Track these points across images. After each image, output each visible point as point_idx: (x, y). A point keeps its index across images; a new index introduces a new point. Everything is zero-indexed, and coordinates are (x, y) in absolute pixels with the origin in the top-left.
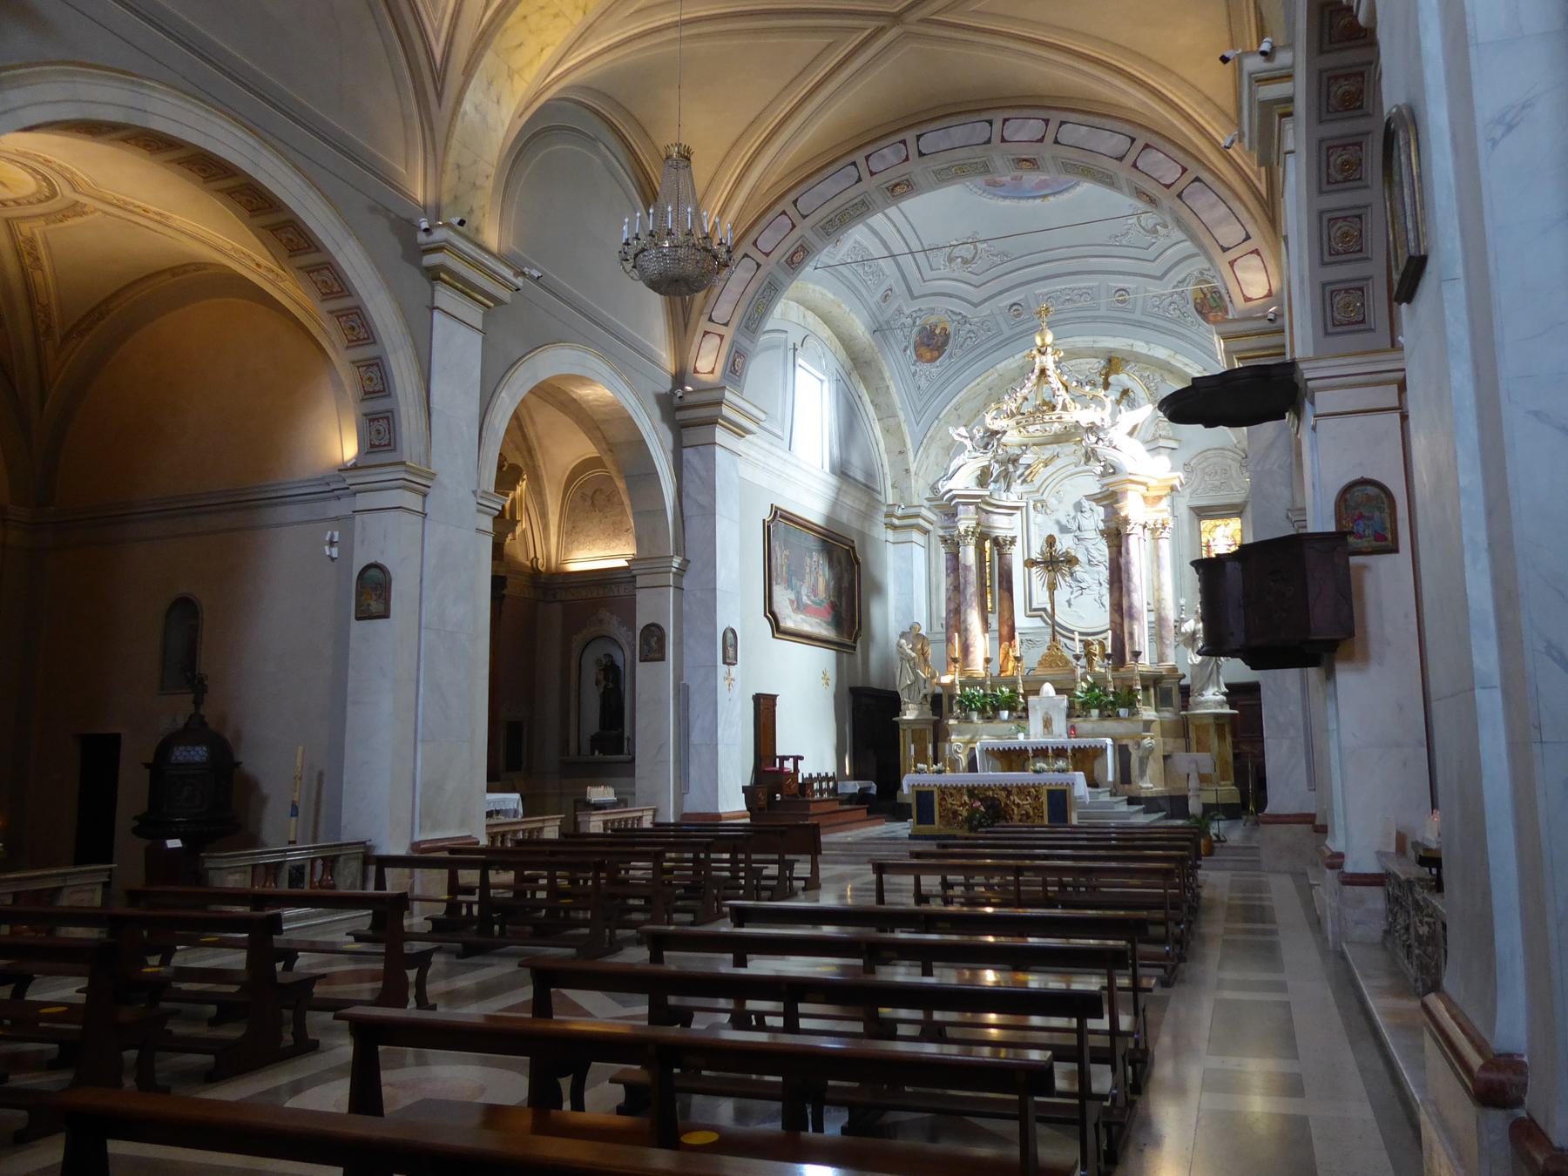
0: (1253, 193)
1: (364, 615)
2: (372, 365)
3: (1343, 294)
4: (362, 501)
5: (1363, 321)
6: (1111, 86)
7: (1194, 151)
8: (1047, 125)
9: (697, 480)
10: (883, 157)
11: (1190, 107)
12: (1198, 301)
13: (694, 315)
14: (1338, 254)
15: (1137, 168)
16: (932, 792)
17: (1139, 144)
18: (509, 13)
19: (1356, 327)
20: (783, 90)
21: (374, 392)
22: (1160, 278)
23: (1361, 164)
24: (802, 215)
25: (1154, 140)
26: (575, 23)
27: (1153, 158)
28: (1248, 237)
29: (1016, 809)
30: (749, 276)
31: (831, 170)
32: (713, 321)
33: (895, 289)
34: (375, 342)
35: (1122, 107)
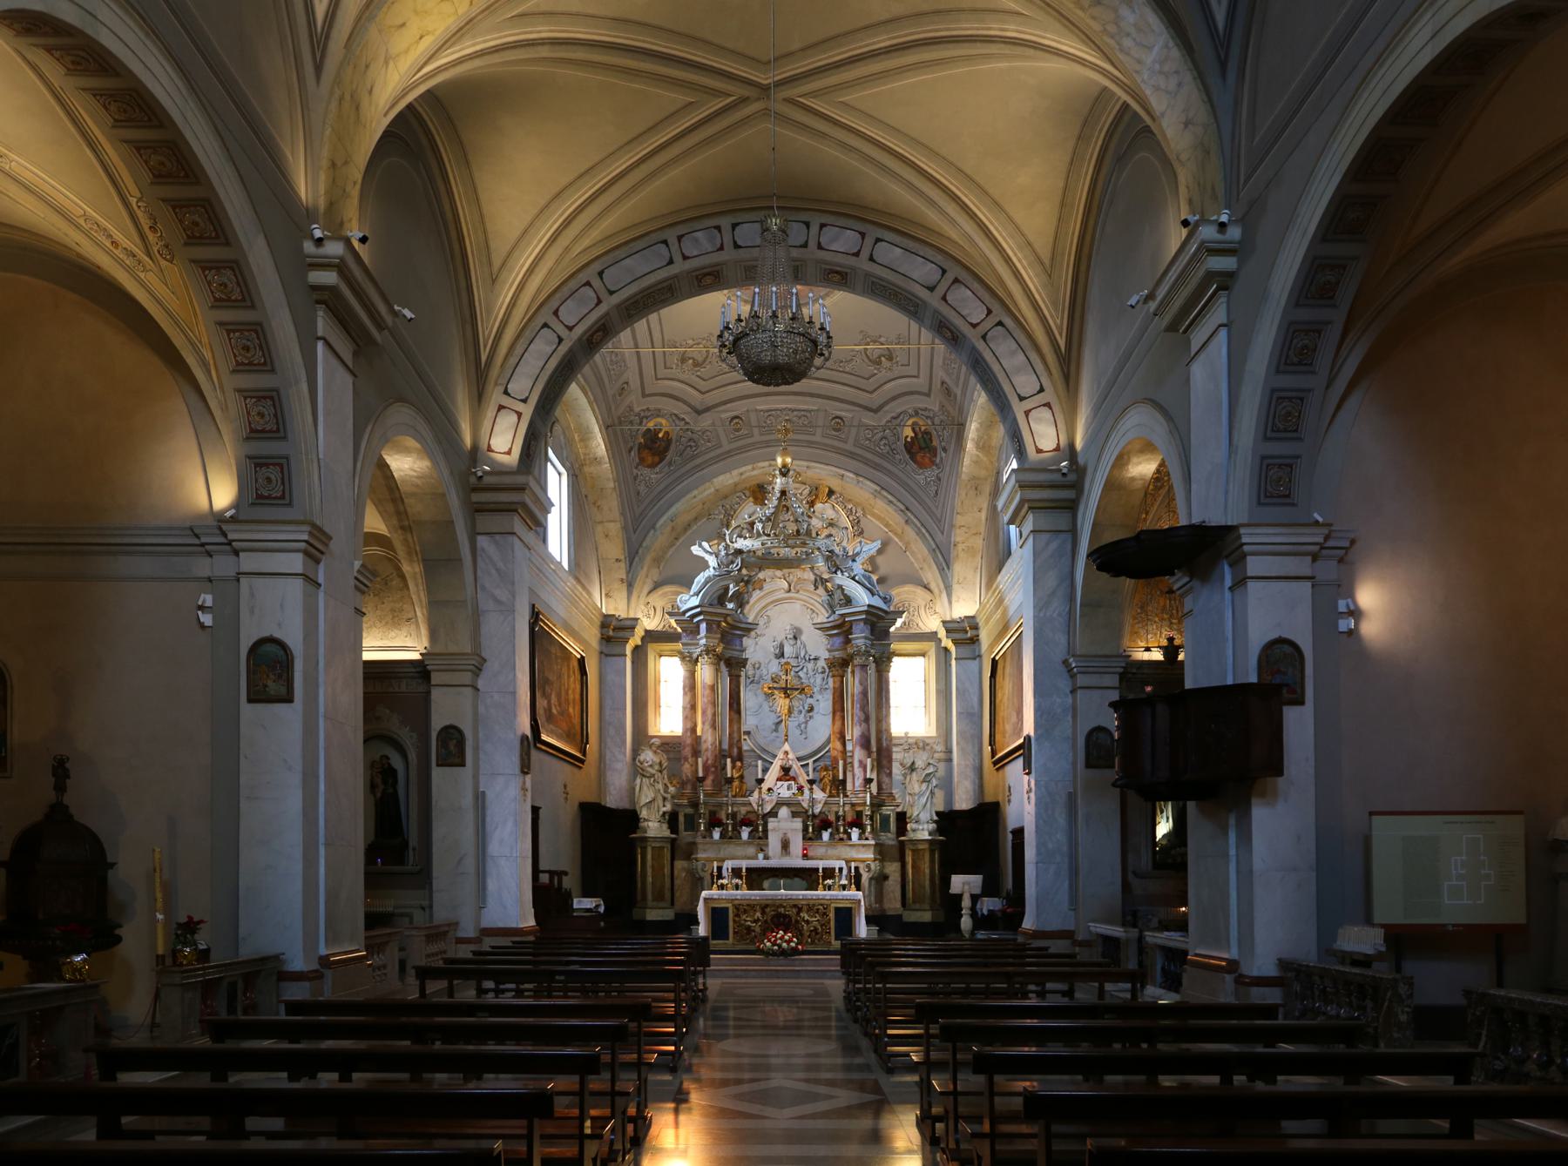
2: (265, 398)
4: (248, 562)
5: (1288, 496)
6: (942, 212)
7: (1001, 293)
8: (863, 239)
9: (494, 571)
10: (696, 240)
12: (909, 439)
16: (727, 909)
17: (950, 277)
20: (626, 144)
21: (263, 431)
22: (875, 411)
23: (1315, 350)
25: (963, 275)
26: (460, 12)
27: (960, 296)
28: (1042, 390)
29: (805, 927)
30: (549, 349)
32: (509, 395)
33: (631, 383)
34: (273, 371)
35: (942, 235)
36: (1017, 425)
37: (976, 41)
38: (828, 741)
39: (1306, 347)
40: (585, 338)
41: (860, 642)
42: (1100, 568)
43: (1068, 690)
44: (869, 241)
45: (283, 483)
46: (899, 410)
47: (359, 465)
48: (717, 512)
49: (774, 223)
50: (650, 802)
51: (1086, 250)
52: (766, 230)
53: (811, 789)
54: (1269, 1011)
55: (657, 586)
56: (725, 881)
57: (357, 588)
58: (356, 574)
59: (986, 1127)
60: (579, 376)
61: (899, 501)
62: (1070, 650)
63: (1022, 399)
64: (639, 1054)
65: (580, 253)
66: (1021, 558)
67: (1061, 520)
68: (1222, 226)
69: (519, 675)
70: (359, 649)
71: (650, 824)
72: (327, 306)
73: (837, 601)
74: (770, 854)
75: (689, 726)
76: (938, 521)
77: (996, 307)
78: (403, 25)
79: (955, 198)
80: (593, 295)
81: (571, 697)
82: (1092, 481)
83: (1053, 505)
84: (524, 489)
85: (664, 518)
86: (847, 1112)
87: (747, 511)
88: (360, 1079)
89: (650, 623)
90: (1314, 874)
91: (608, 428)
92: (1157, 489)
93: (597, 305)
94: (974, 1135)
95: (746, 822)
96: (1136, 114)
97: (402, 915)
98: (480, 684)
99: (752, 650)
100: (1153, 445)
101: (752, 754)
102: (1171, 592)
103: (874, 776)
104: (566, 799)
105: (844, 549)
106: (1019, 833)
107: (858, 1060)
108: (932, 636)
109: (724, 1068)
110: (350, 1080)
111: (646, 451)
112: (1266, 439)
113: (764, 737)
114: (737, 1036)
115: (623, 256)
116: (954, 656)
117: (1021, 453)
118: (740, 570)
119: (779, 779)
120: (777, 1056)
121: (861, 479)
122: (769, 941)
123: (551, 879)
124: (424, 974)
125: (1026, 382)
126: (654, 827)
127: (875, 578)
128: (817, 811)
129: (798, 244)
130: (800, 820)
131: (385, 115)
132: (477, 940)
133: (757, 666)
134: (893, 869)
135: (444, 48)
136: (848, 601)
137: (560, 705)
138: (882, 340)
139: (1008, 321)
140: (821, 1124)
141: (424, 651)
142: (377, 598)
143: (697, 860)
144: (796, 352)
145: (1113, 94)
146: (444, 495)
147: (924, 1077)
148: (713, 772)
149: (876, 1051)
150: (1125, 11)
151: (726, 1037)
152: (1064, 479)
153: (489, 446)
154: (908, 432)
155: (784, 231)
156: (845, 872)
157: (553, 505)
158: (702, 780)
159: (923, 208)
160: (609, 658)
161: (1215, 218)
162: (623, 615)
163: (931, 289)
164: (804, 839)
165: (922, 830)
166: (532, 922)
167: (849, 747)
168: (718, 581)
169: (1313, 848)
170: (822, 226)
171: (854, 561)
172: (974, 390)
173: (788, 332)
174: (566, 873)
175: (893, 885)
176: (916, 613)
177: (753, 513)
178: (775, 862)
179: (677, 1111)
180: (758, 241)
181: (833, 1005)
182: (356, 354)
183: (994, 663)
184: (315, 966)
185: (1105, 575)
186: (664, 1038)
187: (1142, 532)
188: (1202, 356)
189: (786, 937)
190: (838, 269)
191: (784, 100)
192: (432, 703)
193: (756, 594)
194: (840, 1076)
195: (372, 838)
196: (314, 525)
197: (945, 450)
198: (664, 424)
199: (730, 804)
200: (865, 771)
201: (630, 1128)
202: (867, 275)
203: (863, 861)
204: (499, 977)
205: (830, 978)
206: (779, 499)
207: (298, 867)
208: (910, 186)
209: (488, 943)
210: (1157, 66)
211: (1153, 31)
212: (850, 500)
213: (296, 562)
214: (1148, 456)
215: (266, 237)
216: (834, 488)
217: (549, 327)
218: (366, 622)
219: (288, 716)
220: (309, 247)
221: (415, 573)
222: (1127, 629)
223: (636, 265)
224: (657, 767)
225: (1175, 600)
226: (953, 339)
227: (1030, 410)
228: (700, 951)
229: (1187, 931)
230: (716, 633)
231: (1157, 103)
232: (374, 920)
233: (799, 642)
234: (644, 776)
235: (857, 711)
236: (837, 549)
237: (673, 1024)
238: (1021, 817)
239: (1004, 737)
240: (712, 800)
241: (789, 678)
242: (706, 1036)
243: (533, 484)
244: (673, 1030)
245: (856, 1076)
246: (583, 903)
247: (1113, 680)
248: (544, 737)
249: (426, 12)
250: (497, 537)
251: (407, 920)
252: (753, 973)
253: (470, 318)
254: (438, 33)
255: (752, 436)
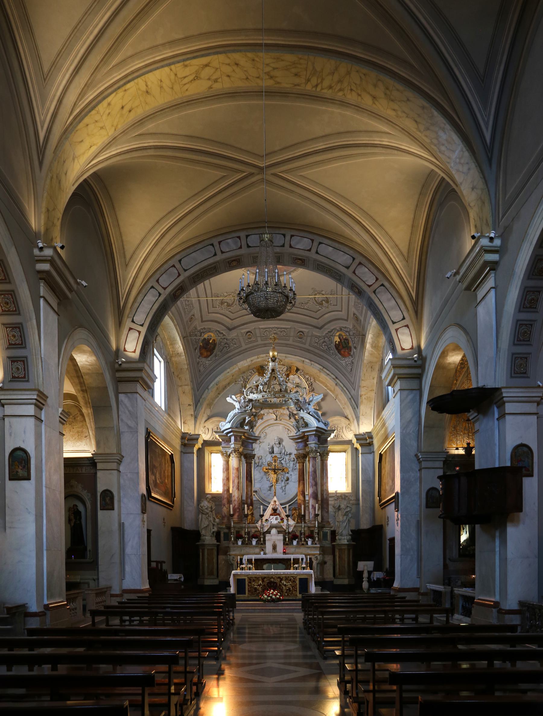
0: (409, 297)
1: (14, 477)
2: (16, 327)
3: (519, 360)
5: (525, 373)
6: (352, 229)
8: (313, 243)
9: (127, 412)
10: (228, 243)
11: (388, 248)
12: (337, 343)
13: (125, 318)
14: (520, 341)
15: (355, 274)
16: (245, 579)
17: (357, 261)
18: (80, 122)
19: (522, 375)
21: (15, 344)
22: (320, 328)
24: (184, 269)
25: (364, 261)
26: (110, 134)
27: (362, 271)
30: (154, 299)
31: (200, 246)
32: (134, 322)
33: (196, 315)
34: (19, 314)
35: (353, 241)
36: (392, 336)
37: (368, 146)
38: (296, 495)
39: (533, 299)
40: (172, 293)
41: (313, 446)
42: (433, 409)
43: (417, 470)
44: (316, 244)
45: (24, 370)
46: (332, 328)
47: (61, 360)
48: (239, 380)
49: (266, 237)
50: (206, 527)
51: (425, 249)
52: (262, 240)
53: (288, 520)
54: (513, 628)
55: (209, 418)
56: (244, 566)
57: (60, 422)
58: (60, 415)
59: (371, 687)
60: (169, 312)
61: (332, 374)
62: (419, 449)
63: (394, 323)
64: (199, 652)
65: (170, 251)
66: (394, 403)
67: (414, 384)
68: (491, 239)
69: (140, 464)
70: (61, 451)
71: (207, 537)
72: (45, 281)
73: (301, 425)
74: (267, 552)
75: (226, 489)
76: (352, 384)
77: (380, 277)
78: (82, 141)
79: (359, 223)
80: (176, 272)
81: (166, 474)
82: (429, 365)
83: (410, 376)
84: (142, 370)
85: (213, 383)
86: (303, 679)
87: (255, 379)
88: (63, 669)
89: (206, 436)
90: (537, 559)
91: (185, 338)
92: (462, 368)
93: (178, 276)
94: (365, 691)
95: (255, 536)
96: (448, 183)
97: (84, 583)
98: (121, 468)
99: (257, 450)
100: (459, 346)
101: (258, 502)
102: (468, 420)
103: (320, 513)
104: (164, 525)
105: (304, 398)
106: (392, 540)
107: (309, 653)
108: (350, 442)
109: (243, 658)
110: (57, 670)
111: (204, 350)
112: (514, 344)
113: (264, 494)
114: (250, 642)
115: (192, 252)
116: (360, 452)
117: (393, 350)
118: (251, 410)
119: (271, 515)
120: (269, 651)
121: (313, 363)
122: (266, 595)
123: (157, 565)
124: (94, 613)
125: (396, 315)
126: (208, 539)
127: (320, 413)
128: (291, 530)
129: (280, 245)
130: (282, 535)
131: (73, 185)
132: (121, 595)
133: (260, 458)
134: (329, 559)
135: (103, 151)
136: (306, 425)
137: (161, 478)
138: (323, 292)
139: (386, 284)
140: (285, 685)
141: (94, 453)
142: (70, 426)
143: (230, 555)
144: (277, 301)
145: (437, 173)
146: (102, 374)
147: (342, 662)
148: (238, 512)
149: (318, 649)
150: (441, 133)
151: (244, 642)
152: (415, 363)
153: (125, 348)
154: (337, 339)
155: (271, 241)
156: (304, 560)
157: (157, 378)
158: (232, 516)
159: (343, 227)
160: (185, 454)
161: (487, 235)
162: (192, 433)
163: (348, 268)
164: (284, 544)
165: (344, 539)
166: (147, 586)
167: (307, 498)
168: (240, 416)
169: (537, 547)
170: (292, 236)
171: (309, 404)
172: (370, 317)
173: (274, 291)
174: (164, 562)
175: (329, 567)
176: (341, 430)
177: (258, 381)
178: (270, 555)
179: (218, 679)
180: (259, 245)
181: (298, 626)
182: (59, 304)
183: (381, 455)
184: (42, 609)
185: (435, 413)
186: (213, 644)
187: (454, 391)
188: (483, 303)
189: (275, 593)
190: (300, 257)
191: (272, 174)
192: (98, 479)
193: (260, 422)
194: (301, 661)
195: (69, 545)
196: (39, 391)
197: (355, 348)
198: (213, 336)
199: (247, 527)
200: (315, 511)
201: (194, 688)
202: (315, 260)
203: (314, 555)
204: (131, 614)
205: (296, 612)
206: (271, 373)
207: (34, 561)
208: (336, 216)
209: (126, 597)
210: (458, 160)
211: (455, 143)
212: (307, 374)
213: (31, 410)
214: (457, 352)
215: (16, 248)
216: (299, 368)
217: (154, 288)
218: (65, 439)
219: (28, 487)
220: (36, 252)
221: (89, 413)
222: (447, 438)
223: (198, 256)
224: (209, 509)
225: (471, 424)
226: (359, 293)
227: (398, 329)
228: (231, 600)
229: (475, 588)
230: (239, 442)
231: (458, 178)
232: (70, 586)
233: (281, 445)
234: (203, 513)
235: (311, 480)
236: (300, 399)
237: (216, 636)
238: (394, 532)
239: (385, 492)
240: (238, 526)
241: (276, 464)
242: (234, 642)
243: (146, 368)
244: (217, 639)
245: (308, 661)
246: (173, 577)
247: (440, 464)
248: (153, 495)
249: (93, 135)
250: (129, 395)
251: (87, 585)
252: (258, 610)
253: (115, 285)
254: (99, 145)
255: (257, 341)
